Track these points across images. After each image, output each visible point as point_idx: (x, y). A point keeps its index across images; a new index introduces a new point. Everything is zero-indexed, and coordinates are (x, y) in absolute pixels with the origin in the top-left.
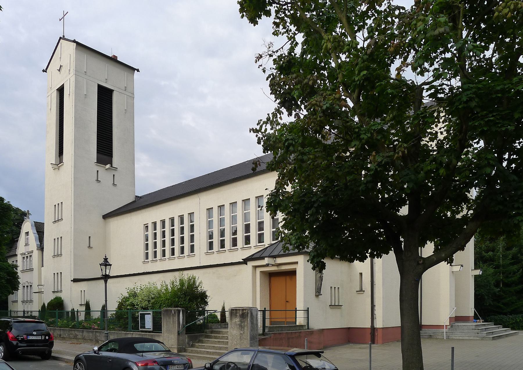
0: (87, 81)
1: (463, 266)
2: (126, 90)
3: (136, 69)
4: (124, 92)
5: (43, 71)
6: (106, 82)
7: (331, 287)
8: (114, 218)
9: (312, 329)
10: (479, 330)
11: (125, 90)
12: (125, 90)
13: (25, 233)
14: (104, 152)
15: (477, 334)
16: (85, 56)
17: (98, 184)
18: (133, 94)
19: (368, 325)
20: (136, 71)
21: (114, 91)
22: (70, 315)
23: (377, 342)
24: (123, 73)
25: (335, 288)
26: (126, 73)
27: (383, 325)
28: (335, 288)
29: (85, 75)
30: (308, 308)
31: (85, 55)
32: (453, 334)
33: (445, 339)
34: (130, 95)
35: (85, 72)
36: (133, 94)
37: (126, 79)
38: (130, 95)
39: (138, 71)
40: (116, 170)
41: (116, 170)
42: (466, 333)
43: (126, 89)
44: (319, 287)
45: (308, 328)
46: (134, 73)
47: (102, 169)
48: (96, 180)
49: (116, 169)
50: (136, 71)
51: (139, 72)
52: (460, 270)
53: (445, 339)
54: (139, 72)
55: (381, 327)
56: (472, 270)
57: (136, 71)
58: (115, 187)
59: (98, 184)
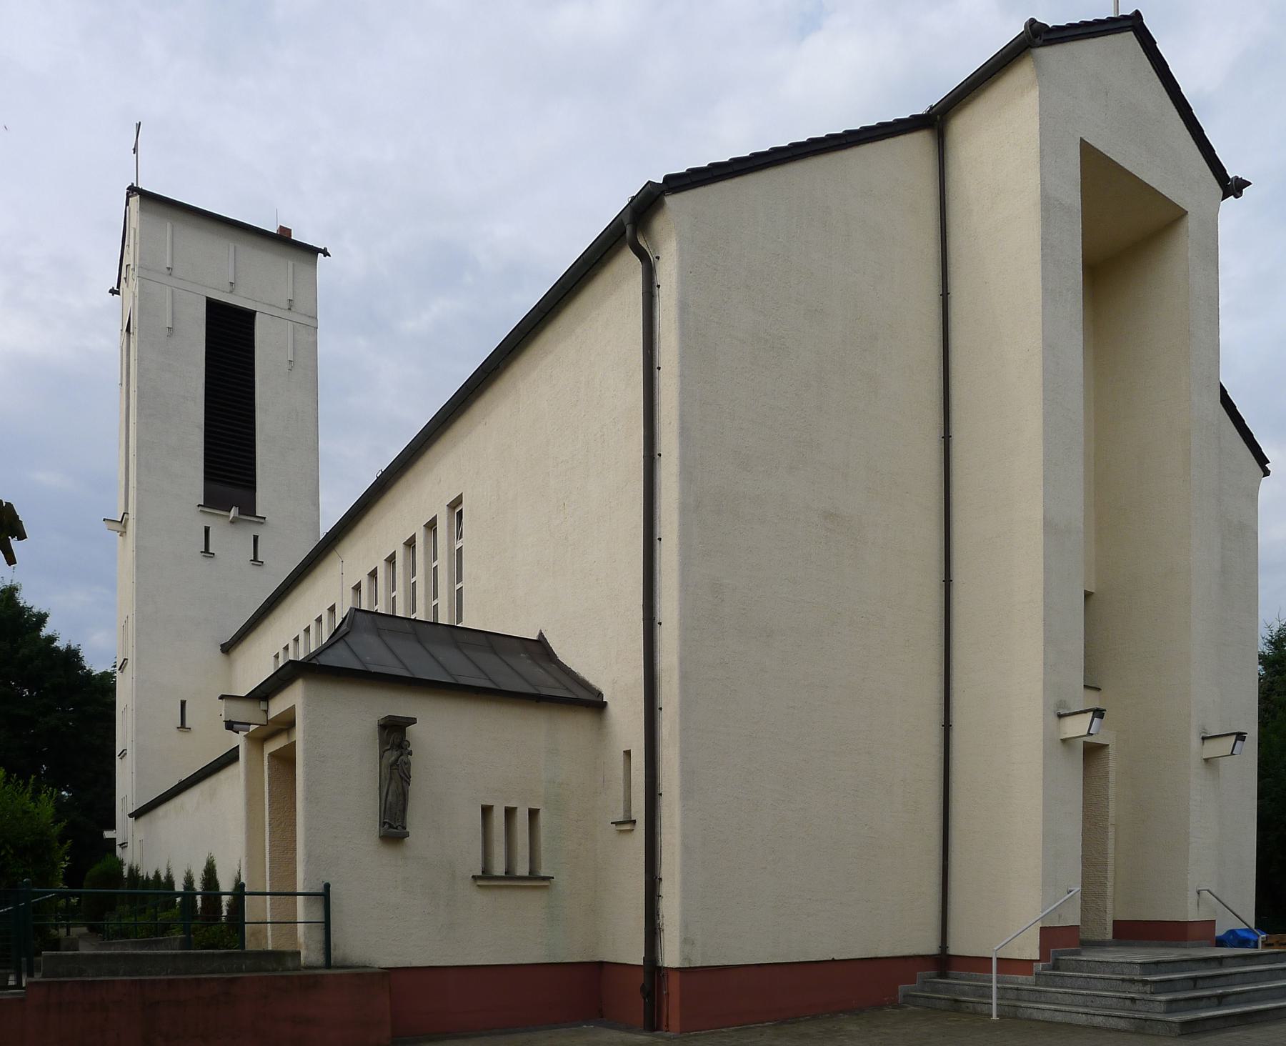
0: (173, 291)
1: (1101, 716)
2: (293, 309)
3: (320, 251)
4: (287, 314)
5: (113, 292)
6: (231, 292)
7: (486, 811)
8: (237, 650)
9: (358, 967)
10: (1148, 988)
11: (289, 309)
12: (289, 309)
13: (624, 751)
14: (224, 477)
15: (1128, 1003)
16: (166, 228)
17: (208, 562)
18: (313, 317)
19: (635, 955)
20: (322, 255)
21: (257, 313)
22: (225, 913)
23: (667, 1026)
24: (280, 265)
25: (510, 812)
26: (290, 263)
27: (686, 958)
28: (510, 812)
29: (170, 277)
30: (327, 886)
31: (169, 224)
32: (1043, 999)
33: (994, 1017)
34: (308, 321)
35: (169, 268)
36: (313, 317)
37: (290, 275)
38: (308, 321)
39: (325, 253)
40: (262, 523)
41: (262, 523)
42: (1089, 999)
43: (291, 306)
44: (388, 803)
45: (328, 964)
46: (316, 265)
47: (219, 524)
48: (202, 552)
49: (262, 521)
50: (319, 254)
51: (329, 255)
52: (1232, 754)
53: (994, 1017)
54: (329, 255)
55: (677, 965)
56: (1204, 739)
57: (319, 254)
58: (258, 567)
59: (209, 561)
